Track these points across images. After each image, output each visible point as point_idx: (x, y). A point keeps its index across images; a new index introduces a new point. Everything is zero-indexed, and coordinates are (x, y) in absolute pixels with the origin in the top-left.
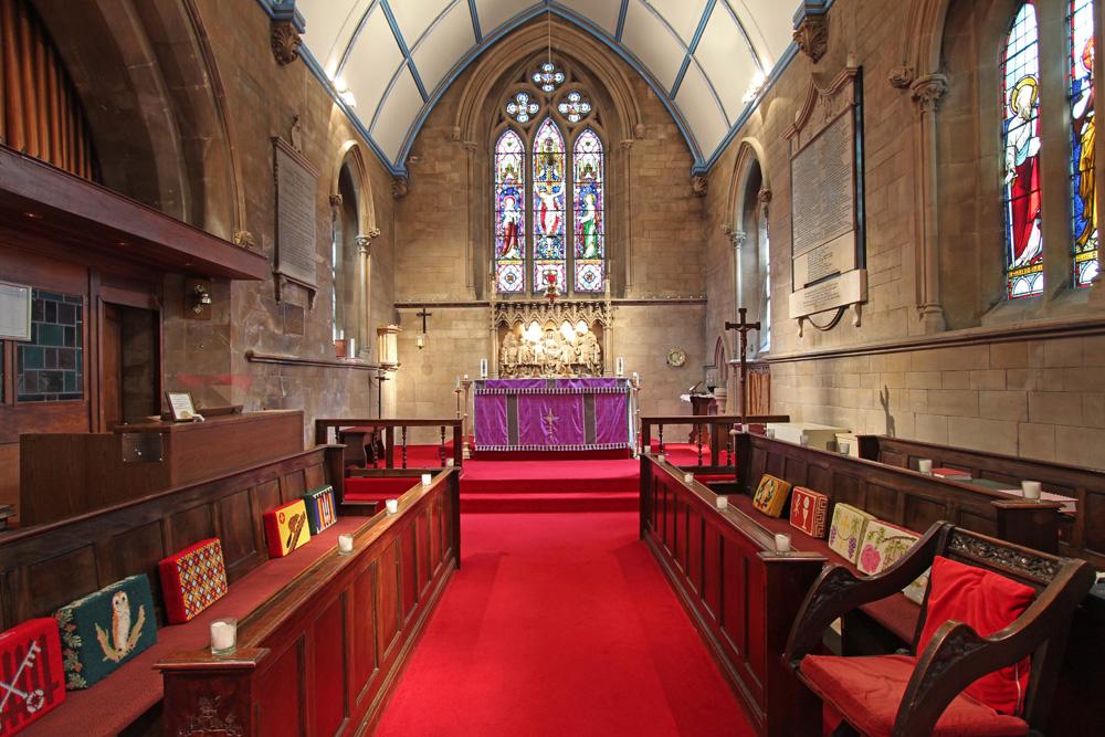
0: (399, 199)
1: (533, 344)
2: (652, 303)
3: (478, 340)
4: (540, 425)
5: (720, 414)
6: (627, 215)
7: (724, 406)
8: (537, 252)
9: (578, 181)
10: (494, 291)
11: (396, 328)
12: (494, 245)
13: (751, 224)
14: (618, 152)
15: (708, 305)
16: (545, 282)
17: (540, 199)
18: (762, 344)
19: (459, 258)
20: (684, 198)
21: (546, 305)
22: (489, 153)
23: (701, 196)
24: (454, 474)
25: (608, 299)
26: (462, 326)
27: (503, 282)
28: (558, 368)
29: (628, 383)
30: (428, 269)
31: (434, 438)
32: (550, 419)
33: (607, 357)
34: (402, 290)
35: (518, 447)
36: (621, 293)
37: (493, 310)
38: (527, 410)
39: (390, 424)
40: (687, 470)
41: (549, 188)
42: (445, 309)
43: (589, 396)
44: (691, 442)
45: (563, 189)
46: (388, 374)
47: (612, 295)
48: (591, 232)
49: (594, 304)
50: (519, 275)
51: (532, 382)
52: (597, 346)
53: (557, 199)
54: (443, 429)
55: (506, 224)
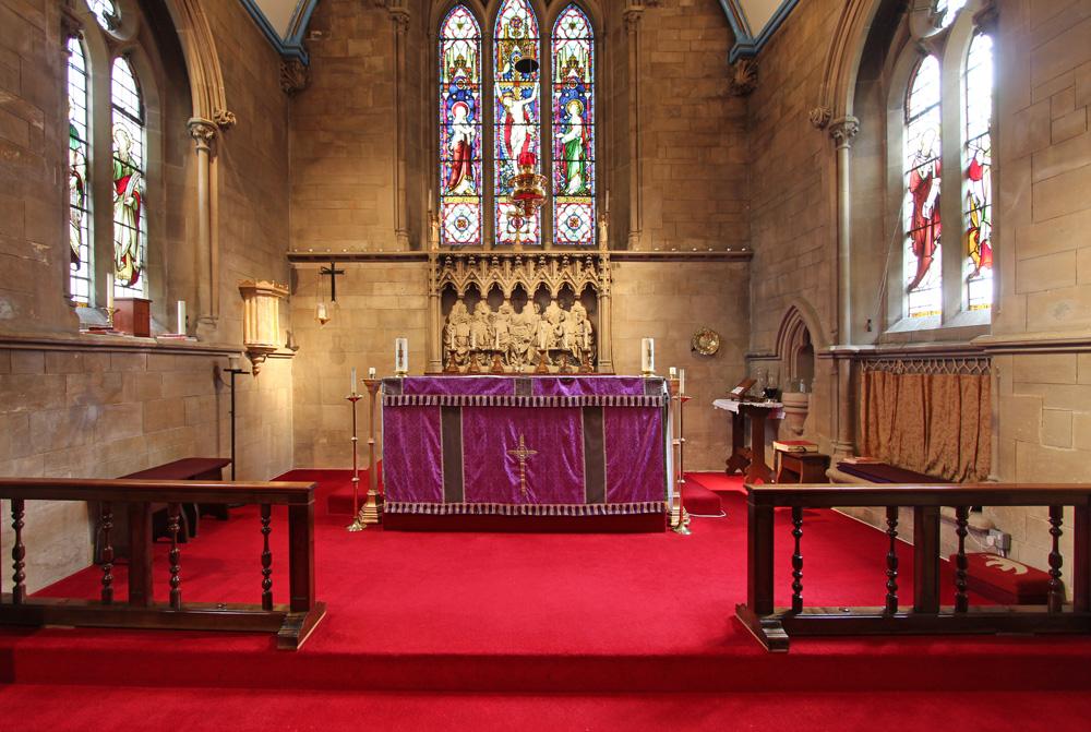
0: (294, 93)
1: (524, 362)
2: (670, 258)
6: (632, 124)
8: (500, 185)
9: (558, 81)
12: (438, 175)
13: (870, 104)
14: (617, 32)
15: (755, 262)
16: (512, 229)
17: (504, 107)
18: (891, 319)
19: (384, 186)
20: (719, 97)
22: (433, 39)
23: (745, 92)
25: (604, 252)
26: (388, 290)
27: (451, 229)
28: (530, 356)
30: (338, 204)
33: (604, 340)
34: (300, 235)
35: (463, 506)
37: (434, 265)
38: (478, 437)
41: (518, 91)
43: (592, 411)
45: (536, 94)
48: (576, 157)
49: (583, 259)
50: (474, 219)
52: (588, 323)
53: (527, 108)
55: (455, 144)
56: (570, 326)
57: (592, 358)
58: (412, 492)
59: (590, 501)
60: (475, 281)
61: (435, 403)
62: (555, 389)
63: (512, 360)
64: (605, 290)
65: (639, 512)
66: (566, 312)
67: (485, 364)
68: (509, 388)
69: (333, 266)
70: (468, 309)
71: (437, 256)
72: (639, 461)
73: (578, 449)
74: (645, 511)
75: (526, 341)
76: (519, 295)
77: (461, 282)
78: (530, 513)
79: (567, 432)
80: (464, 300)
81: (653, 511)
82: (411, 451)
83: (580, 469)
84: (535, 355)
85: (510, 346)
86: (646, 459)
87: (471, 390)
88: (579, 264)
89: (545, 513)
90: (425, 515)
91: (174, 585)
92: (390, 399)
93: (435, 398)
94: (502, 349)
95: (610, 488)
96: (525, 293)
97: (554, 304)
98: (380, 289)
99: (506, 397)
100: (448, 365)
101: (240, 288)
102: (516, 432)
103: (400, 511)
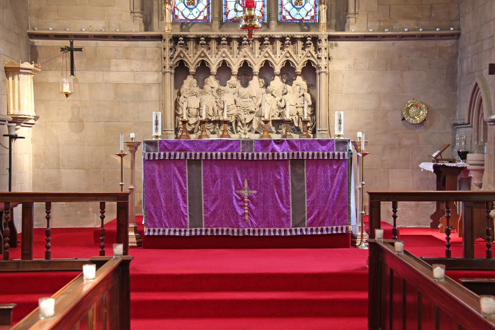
1: (250, 131)
3: (149, 86)
4: (231, 202)
5: (475, 189)
7: (481, 178)
10: (169, 18)
11: (32, 66)
15: (461, 39)
16: (240, 8)
21: (240, 40)
24: (124, 265)
25: (323, 33)
26: (124, 66)
28: (255, 126)
29: (351, 146)
31: (90, 218)
32: (245, 193)
33: (322, 111)
34: (39, 14)
35: (203, 230)
36: (341, 24)
37: (168, 45)
38: (214, 181)
39: (27, 200)
40: (438, 262)
42: (101, 43)
43: (297, 162)
44: (434, 226)
46: (21, 131)
47: (329, 26)
49: (304, 39)
51: (222, 144)
52: (308, 96)
54: (103, 207)
56: (292, 99)
57: (311, 127)
58: (165, 221)
59: (295, 226)
60: (205, 59)
61: (183, 157)
62: (270, 147)
63: (239, 129)
64: (323, 68)
65: (330, 233)
66: (288, 86)
67: (213, 133)
68: (237, 147)
69: (72, 43)
70: (198, 83)
71: (171, 37)
72: (330, 197)
73: (287, 189)
74: (334, 232)
75: (251, 112)
76: (246, 71)
77: (192, 60)
78: (251, 234)
79: (279, 178)
80: (195, 76)
81: (339, 232)
82: (165, 192)
83: (288, 203)
84: (260, 124)
85: (237, 117)
86: (335, 196)
87: (209, 148)
88: (300, 44)
89: (262, 234)
90: (175, 236)
91: (48, 248)
92: (149, 155)
93: (183, 154)
94: (229, 119)
95: (309, 216)
96: (251, 69)
97: (277, 79)
98: (117, 65)
99: (235, 153)
100: (180, 134)
101: (5, 68)
102: (242, 177)
103: (156, 234)
